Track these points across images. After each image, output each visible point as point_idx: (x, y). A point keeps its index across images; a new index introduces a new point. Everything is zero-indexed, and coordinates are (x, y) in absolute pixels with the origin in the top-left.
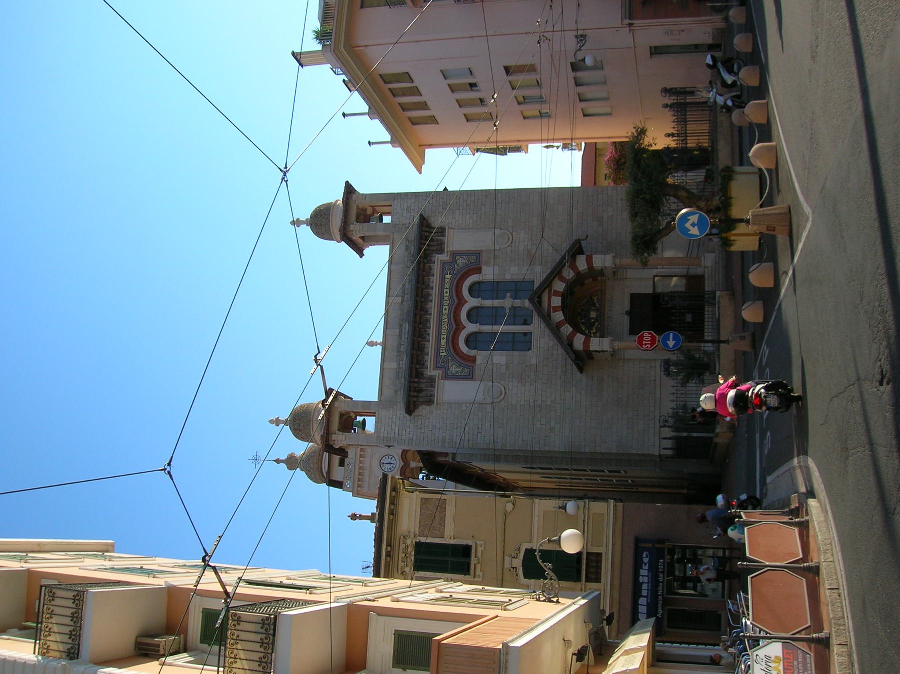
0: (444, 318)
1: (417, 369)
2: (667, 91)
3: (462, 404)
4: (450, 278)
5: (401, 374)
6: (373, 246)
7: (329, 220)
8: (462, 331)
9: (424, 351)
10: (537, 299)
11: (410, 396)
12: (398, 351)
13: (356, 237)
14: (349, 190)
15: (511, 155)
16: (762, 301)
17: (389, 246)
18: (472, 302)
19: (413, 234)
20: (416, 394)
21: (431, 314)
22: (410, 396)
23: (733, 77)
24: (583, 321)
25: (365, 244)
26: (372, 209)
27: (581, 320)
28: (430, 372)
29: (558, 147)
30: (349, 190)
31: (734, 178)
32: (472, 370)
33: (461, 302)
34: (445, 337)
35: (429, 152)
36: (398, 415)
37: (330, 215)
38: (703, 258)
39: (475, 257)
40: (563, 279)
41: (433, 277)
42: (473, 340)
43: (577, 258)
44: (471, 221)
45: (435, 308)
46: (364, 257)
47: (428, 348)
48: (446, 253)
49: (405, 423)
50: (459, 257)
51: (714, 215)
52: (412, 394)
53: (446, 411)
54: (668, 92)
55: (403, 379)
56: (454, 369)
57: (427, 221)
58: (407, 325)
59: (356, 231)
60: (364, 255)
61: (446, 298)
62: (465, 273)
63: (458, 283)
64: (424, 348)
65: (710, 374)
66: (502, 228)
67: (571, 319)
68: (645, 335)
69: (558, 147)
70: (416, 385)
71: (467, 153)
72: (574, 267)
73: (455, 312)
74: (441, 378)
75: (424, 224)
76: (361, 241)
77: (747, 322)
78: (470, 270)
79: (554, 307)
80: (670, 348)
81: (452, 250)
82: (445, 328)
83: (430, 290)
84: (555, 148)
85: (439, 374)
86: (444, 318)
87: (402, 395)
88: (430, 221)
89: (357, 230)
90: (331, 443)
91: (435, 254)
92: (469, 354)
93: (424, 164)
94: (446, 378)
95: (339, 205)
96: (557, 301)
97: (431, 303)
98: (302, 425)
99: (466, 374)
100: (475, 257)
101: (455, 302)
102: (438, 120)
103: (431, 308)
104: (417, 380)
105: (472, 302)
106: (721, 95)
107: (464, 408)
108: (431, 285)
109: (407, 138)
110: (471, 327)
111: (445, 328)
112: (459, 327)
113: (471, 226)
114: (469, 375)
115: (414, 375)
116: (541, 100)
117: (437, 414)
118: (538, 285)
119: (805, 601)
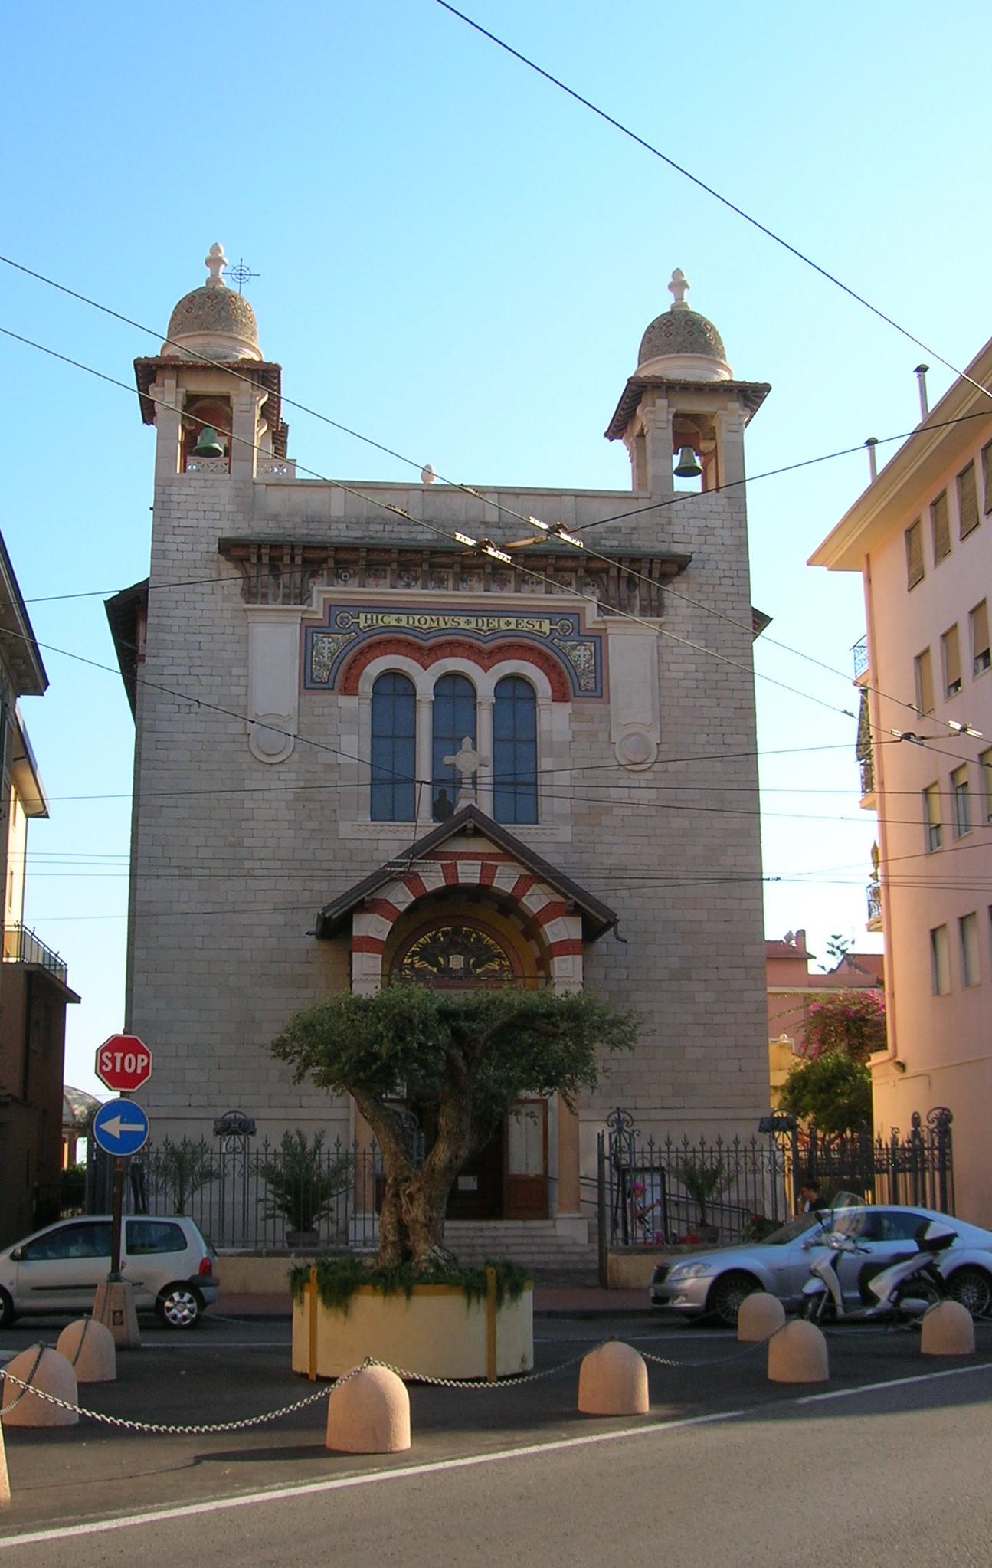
0: (447, 618)
1: (325, 561)
2: (944, 1120)
3: (246, 666)
4: (543, 630)
5: (315, 525)
6: (629, 459)
7: (678, 352)
8: (417, 661)
9: (369, 576)
10: (470, 826)
11: (260, 547)
12: (369, 518)
13: (643, 414)
14: (752, 395)
15: (856, 769)
16: (113, 1376)
17: (630, 489)
18: (485, 682)
19: (646, 543)
20: (266, 560)
21: (456, 589)
22: (260, 547)
23: (887, 1292)
24: (442, 939)
25: (631, 439)
26: (711, 449)
27: (445, 934)
28: (319, 592)
29: (874, 876)
30: (752, 395)
31: (474, 1300)
32: (326, 686)
33: (487, 658)
34: (403, 623)
35: (857, 578)
36: (220, 524)
37: (693, 352)
38: (577, 1215)
39: (591, 685)
40: (523, 884)
41: (544, 591)
42: (396, 685)
43: (575, 918)
44: (681, 675)
45: (471, 597)
46: (607, 440)
47: (377, 586)
48: (600, 619)
49: (202, 540)
50: (593, 649)
51: (393, 1243)
52: (296, 552)
53: (229, 630)
54: (940, 1125)
55: (305, 531)
56: (327, 645)
57: (678, 573)
58: (429, 536)
59: (652, 412)
60: (611, 441)
61: (494, 623)
62: (555, 666)
63: (531, 649)
64: (375, 576)
65: (288, 1233)
66: (663, 748)
67: (425, 902)
68: (140, 1056)
69: (874, 876)
70: (287, 560)
71: (858, 667)
72: (551, 912)
73: (461, 644)
74: (306, 616)
75: (673, 566)
76: (637, 430)
77: (60, 1333)
78: (560, 674)
79: (455, 865)
80: (99, 1122)
81: (609, 631)
82: (425, 622)
83: (513, 585)
84: (873, 870)
85: (315, 612)
86: (447, 618)
87: (269, 531)
88: (677, 579)
89: (656, 415)
90: (646, 398)
91: (598, 595)
92: (361, 679)
93: (830, 570)
94: (306, 627)
95: (717, 373)
96: (469, 873)
97: (482, 589)
98: (201, 313)
99: (315, 673)
100: (591, 685)
101: (484, 642)
102: (917, 588)
103: (471, 589)
104: (298, 560)
105: (485, 682)
106: (834, 1262)
107: (235, 671)
108: (525, 587)
109: (877, 516)
110: (425, 681)
111: (425, 622)
112: (426, 654)
113: (667, 675)
114: (312, 681)
115: (310, 555)
116: (962, 826)
117: (222, 610)
118: (509, 831)
119: (895, 1379)
